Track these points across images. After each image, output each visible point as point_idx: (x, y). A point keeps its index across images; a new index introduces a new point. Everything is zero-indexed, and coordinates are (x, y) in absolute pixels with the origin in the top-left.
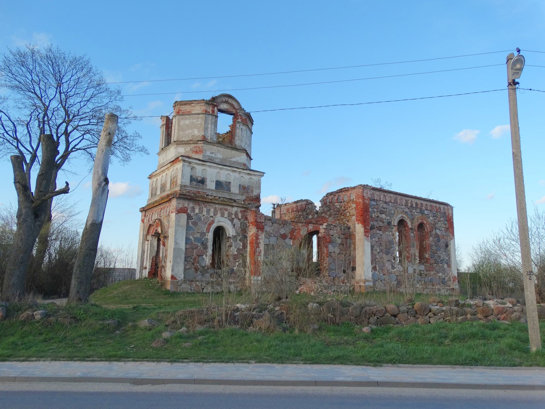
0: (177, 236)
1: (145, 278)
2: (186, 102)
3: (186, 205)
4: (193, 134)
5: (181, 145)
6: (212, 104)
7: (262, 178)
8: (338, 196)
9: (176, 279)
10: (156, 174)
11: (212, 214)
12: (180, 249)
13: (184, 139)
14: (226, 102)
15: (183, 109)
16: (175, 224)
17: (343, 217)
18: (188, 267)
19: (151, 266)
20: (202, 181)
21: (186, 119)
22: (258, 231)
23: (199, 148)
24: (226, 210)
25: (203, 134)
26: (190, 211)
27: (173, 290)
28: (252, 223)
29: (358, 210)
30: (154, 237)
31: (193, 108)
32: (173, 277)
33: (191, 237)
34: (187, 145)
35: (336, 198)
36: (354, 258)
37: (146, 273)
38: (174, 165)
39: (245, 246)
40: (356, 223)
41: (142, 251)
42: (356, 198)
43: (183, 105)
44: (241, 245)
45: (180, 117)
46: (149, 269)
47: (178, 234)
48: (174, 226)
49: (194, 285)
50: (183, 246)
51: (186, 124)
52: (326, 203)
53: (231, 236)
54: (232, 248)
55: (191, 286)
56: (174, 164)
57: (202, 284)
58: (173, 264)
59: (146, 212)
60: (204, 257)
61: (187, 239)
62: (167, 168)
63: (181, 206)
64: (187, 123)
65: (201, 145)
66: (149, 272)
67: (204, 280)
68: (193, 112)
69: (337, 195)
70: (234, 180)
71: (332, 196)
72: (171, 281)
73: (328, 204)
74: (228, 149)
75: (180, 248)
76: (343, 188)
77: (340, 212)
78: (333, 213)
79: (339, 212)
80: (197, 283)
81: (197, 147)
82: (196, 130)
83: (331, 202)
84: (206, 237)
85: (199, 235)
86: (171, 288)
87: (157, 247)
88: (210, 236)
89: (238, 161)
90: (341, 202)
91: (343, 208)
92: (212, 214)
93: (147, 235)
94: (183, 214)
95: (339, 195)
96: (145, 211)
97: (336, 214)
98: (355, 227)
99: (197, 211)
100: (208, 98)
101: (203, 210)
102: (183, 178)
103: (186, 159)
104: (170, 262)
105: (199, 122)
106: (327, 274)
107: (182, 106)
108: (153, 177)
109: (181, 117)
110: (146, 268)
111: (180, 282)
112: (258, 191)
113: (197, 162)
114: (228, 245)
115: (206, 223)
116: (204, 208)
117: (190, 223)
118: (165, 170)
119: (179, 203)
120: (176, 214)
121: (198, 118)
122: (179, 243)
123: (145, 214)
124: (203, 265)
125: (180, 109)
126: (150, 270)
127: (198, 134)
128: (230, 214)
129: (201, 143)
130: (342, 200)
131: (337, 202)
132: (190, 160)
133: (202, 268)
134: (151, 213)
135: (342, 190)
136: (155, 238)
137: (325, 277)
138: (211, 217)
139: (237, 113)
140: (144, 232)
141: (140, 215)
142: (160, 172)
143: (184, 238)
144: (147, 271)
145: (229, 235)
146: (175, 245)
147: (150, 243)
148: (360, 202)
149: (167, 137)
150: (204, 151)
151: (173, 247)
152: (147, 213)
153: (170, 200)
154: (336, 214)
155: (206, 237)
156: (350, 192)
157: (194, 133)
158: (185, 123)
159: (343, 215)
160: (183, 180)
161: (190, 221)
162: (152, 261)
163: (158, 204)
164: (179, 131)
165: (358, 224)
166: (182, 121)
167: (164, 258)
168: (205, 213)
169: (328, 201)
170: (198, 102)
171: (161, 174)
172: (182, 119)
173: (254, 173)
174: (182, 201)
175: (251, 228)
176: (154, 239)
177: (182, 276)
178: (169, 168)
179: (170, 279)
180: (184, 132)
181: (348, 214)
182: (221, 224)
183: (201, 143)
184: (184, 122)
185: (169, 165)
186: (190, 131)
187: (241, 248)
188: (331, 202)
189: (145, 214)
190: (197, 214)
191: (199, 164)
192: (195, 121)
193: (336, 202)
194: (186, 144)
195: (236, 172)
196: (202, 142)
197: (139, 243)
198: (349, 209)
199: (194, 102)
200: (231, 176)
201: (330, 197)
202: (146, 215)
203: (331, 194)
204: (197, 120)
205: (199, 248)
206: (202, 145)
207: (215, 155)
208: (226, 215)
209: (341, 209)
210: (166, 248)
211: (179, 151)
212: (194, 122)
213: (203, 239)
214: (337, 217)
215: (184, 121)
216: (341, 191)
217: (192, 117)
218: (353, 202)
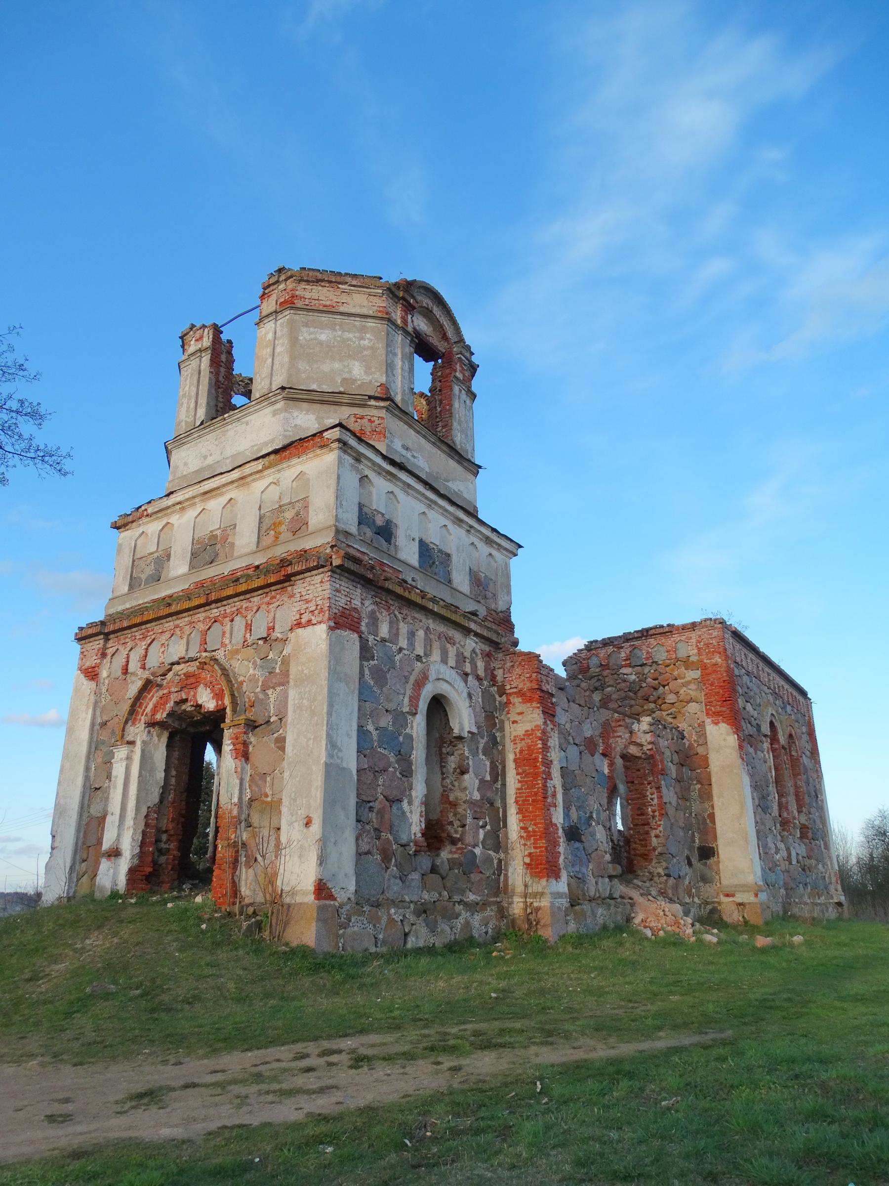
0: (334, 715)
1: (115, 895)
2: (320, 276)
3: (357, 603)
4: (346, 376)
5: (305, 405)
6: (403, 298)
7: (514, 562)
8: (630, 649)
9: (331, 897)
10: (168, 508)
11: (420, 651)
12: (344, 768)
13: (314, 387)
14: (427, 314)
15: (307, 295)
16: (330, 668)
17: (652, 705)
18: (365, 847)
19: (142, 845)
20: (386, 532)
21: (322, 326)
22: (545, 723)
23: (370, 420)
24: (450, 640)
25: (383, 380)
26: (367, 626)
27: (327, 947)
28: (520, 694)
29: (712, 685)
30: (155, 731)
31: (344, 298)
32: (322, 890)
33: (370, 727)
34: (326, 407)
35: (623, 655)
36: (705, 823)
37: (115, 875)
38: (280, 467)
39: (498, 774)
40: (708, 721)
41: (84, 786)
42: (699, 654)
43: (308, 282)
44: (488, 770)
45: (297, 317)
46: (133, 857)
47: (336, 707)
48: (324, 674)
49: (384, 919)
50: (350, 760)
51: (321, 343)
52: (589, 668)
53: (466, 735)
54: (466, 777)
55: (374, 926)
56: (281, 461)
57: (404, 916)
58: (323, 834)
59: (107, 640)
60: (405, 804)
61: (362, 731)
62: (242, 478)
63: (342, 601)
64: (323, 337)
65: (375, 412)
66: (132, 871)
67: (407, 898)
68: (342, 309)
69: (627, 645)
70: (458, 549)
71: (610, 649)
72: (320, 909)
73: (594, 670)
74: (439, 448)
75: (345, 765)
76: (651, 625)
77: (640, 694)
78: (614, 696)
79: (635, 693)
80: (393, 911)
81: (362, 418)
82: (357, 363)
83: (607, 665)
84: (407, 731)
85: (389, 718)
86: (318, 939)
87: (165, 771)
88: (418, 726)
89: (462, 492)
90: (642, 665)
91: (649, 680)
92: (420, 651)
93: (126, 722)
94: (348, 632)
95: (635, 648)
96: (107, 636)
97: (626, 698)
98: (702, 734)
99: (384, 630)
100: (392, 277)
101: (398, 629)
102: (341, 505)
103: (352, 442)
104: (308, 824)
105: (365, 343)
106: (660, 871)
107: (303, 285)
108: (145, 520)
109: (300, 317)
110: (115, 853)
111: (343, 911)
112: (506, 597)
113: (379, 460)
114: (453, 766)
115: (407, 679)
116: (401, 624)
117: (367, 672)
118: (224, 485)
119: (338, 591)
120: (331, 629)
121: (363, 330)
122: (339, 744)
123: (105, 648)
124: (404, 838)
125: (297, 293)
126: (136, 861)
127: (367, 379)
128: (461, 658)
129: (377, 407)
130: (647, 659)
131: (630, 666)
132: (362, 449)
133: (401, 849)
134: (144, 644)
135: (651, 632)
136: (159, 736)
137: (656, 879)
138: (419, 658)
139: (451, 353)
140: (98, 713)
141: (76, 648)
142: (194, 497)
143: (355, 727)
144: (124, 865)
145: (462, 729)
146: (330, 755)
147: (143, 751)
148: (715, 665)
149: (213, 391)
150: (387, 435)
151: (323, 759)
152: (110, 643)
153: (288, 578)
154: (626, 698)
155: (407, 731)
156: (676, 638)
157: (350, 372)
158: (315, 339)
159: (655, 702)
160: (340, 510)
161: (366, 663)
162: (147, 825)
163: (202, 600)
164: (293, 358)
165: (716, 724)
166: (304, 329)
167: (244, 808)
168: (403, 643)
169: (594, 661)
170: (365, 282)
171: (194, 504)
172: (306, 325)
173: (498, 540)
174: (345, 585)
175: (518, 710)
176: (156, 738)
177: (352, 888)
178: (249, 479)
179: (312, 897)
180: (315, 366)
181: (671, 698)
182: (444, 688)
183: (377, 407)
184: (311, 334)
185: (259, 465)
186: (337, 365)
187: (488, 778)
188: (607, 665)
189: (105, 648)
190: (384, 640)
191: (380, 471)
192: (351, 335)
193: (625, 666)
194: (322, 402)
195: (460, 526)
196: (382, 404)
197: (66, 757)
198: (673, 685)
199: (349, 279)
200: (450, 534)
201: (602, 653)
202: (110, 651)
203: (607, 642)
204: (357, 335)
205: (391, 769)
206: (383, 413)
207: (414, 456)
208: (452, 662)
209: (644, 685)
210: (254, 767)
211: (298, 422)
212: (349, 339)
213: (401, 739)
214: (631, 706)
215: (312, 329)
216: (645, 634)
217: (341, 325)
218: (687, 663)
